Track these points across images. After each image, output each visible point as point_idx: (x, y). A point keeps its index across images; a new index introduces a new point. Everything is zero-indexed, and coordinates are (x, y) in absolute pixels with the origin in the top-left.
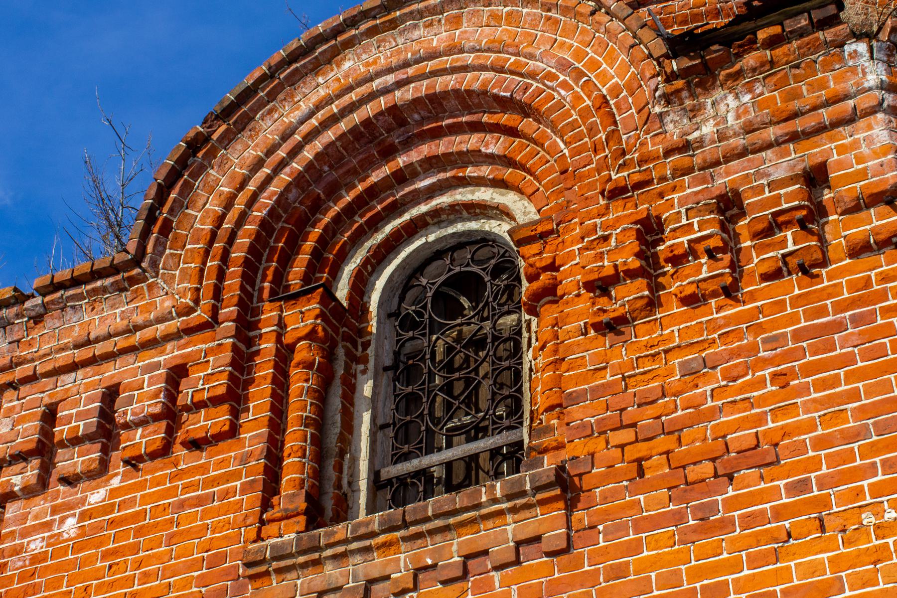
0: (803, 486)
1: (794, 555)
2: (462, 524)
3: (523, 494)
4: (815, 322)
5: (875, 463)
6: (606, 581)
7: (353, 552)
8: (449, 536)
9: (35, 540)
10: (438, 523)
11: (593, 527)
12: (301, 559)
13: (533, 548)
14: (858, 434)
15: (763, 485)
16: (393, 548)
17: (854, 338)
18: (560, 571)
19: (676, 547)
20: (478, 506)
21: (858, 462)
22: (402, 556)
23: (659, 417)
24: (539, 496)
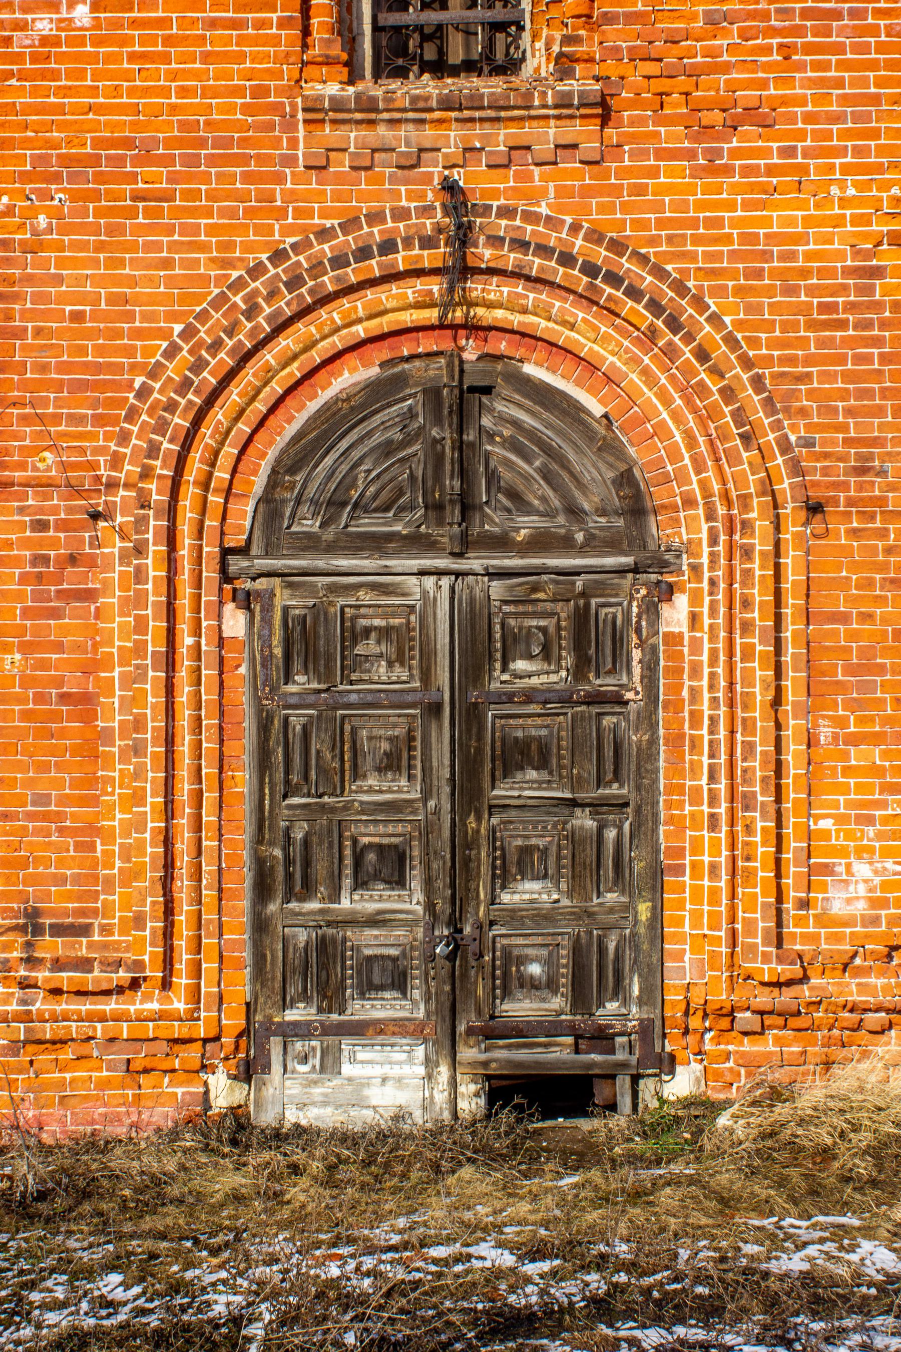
0: (788, 152)
1: (776, 206)
2: (512, 119)
3: (570, 106)
4: (820, 5)
5: (847, 146)
6: (629, 196)
7: (407, 120)
8: (497, 126)
9: (41, 19)
10: (491, 113)
11: (619, 146)
12: (358, 116)
13: (568, 152)
14: (839, 119)
15: (760, 143)
16: (444, 125)
17: (849, 30)
18: (590, 178)
19: (687, 180)
20: (528, 108)
21: (835, 143)
22: (452, 134)
23: (681, 59)
24: (583, 111)
